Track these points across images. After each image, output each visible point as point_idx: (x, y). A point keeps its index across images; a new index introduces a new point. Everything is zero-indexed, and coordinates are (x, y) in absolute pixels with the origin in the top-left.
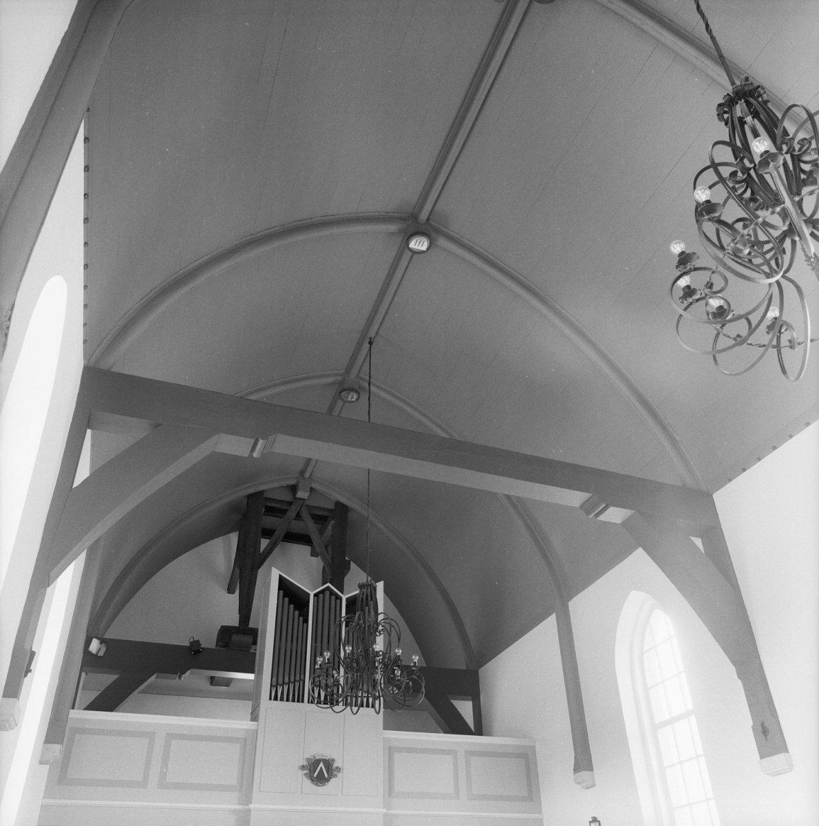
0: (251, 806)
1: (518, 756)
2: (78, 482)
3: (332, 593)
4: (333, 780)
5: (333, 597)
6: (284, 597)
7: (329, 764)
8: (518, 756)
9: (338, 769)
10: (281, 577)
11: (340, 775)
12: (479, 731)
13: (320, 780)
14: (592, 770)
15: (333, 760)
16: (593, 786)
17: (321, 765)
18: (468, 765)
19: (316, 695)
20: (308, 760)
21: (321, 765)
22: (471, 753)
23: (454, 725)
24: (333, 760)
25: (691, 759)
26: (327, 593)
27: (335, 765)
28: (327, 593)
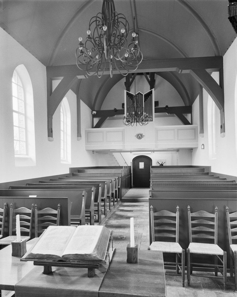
0: (125, 144)
1: (192, 129)
2: (198, 97)
3: (141, 94)
4: (143, 138)
5: (141, 95)
6: (128, 97)
7: (141, 135)
8: (192, 129)
9: (144, 136)
10: (127, 92)
11: (144, 137)
12: (192, 124)
13: (140, 138)
14: (203, 133)
15: (142, 134)
16: (203, 137)
17: (140, 135)
18: (178, 132)
19: (147, 119)
20: (137, 134)
21: (140, 135)
22: (178, 130)
23: (186, 122)
24: (142, 134)
25: (159, 163)
26: (139, 94)
27: (143, 135)
28: (139, 94)
